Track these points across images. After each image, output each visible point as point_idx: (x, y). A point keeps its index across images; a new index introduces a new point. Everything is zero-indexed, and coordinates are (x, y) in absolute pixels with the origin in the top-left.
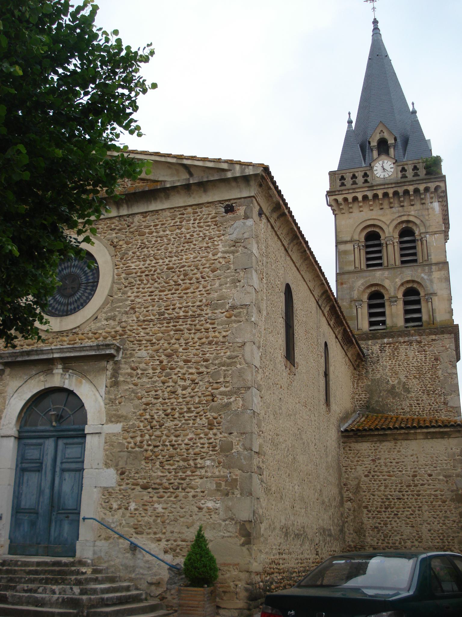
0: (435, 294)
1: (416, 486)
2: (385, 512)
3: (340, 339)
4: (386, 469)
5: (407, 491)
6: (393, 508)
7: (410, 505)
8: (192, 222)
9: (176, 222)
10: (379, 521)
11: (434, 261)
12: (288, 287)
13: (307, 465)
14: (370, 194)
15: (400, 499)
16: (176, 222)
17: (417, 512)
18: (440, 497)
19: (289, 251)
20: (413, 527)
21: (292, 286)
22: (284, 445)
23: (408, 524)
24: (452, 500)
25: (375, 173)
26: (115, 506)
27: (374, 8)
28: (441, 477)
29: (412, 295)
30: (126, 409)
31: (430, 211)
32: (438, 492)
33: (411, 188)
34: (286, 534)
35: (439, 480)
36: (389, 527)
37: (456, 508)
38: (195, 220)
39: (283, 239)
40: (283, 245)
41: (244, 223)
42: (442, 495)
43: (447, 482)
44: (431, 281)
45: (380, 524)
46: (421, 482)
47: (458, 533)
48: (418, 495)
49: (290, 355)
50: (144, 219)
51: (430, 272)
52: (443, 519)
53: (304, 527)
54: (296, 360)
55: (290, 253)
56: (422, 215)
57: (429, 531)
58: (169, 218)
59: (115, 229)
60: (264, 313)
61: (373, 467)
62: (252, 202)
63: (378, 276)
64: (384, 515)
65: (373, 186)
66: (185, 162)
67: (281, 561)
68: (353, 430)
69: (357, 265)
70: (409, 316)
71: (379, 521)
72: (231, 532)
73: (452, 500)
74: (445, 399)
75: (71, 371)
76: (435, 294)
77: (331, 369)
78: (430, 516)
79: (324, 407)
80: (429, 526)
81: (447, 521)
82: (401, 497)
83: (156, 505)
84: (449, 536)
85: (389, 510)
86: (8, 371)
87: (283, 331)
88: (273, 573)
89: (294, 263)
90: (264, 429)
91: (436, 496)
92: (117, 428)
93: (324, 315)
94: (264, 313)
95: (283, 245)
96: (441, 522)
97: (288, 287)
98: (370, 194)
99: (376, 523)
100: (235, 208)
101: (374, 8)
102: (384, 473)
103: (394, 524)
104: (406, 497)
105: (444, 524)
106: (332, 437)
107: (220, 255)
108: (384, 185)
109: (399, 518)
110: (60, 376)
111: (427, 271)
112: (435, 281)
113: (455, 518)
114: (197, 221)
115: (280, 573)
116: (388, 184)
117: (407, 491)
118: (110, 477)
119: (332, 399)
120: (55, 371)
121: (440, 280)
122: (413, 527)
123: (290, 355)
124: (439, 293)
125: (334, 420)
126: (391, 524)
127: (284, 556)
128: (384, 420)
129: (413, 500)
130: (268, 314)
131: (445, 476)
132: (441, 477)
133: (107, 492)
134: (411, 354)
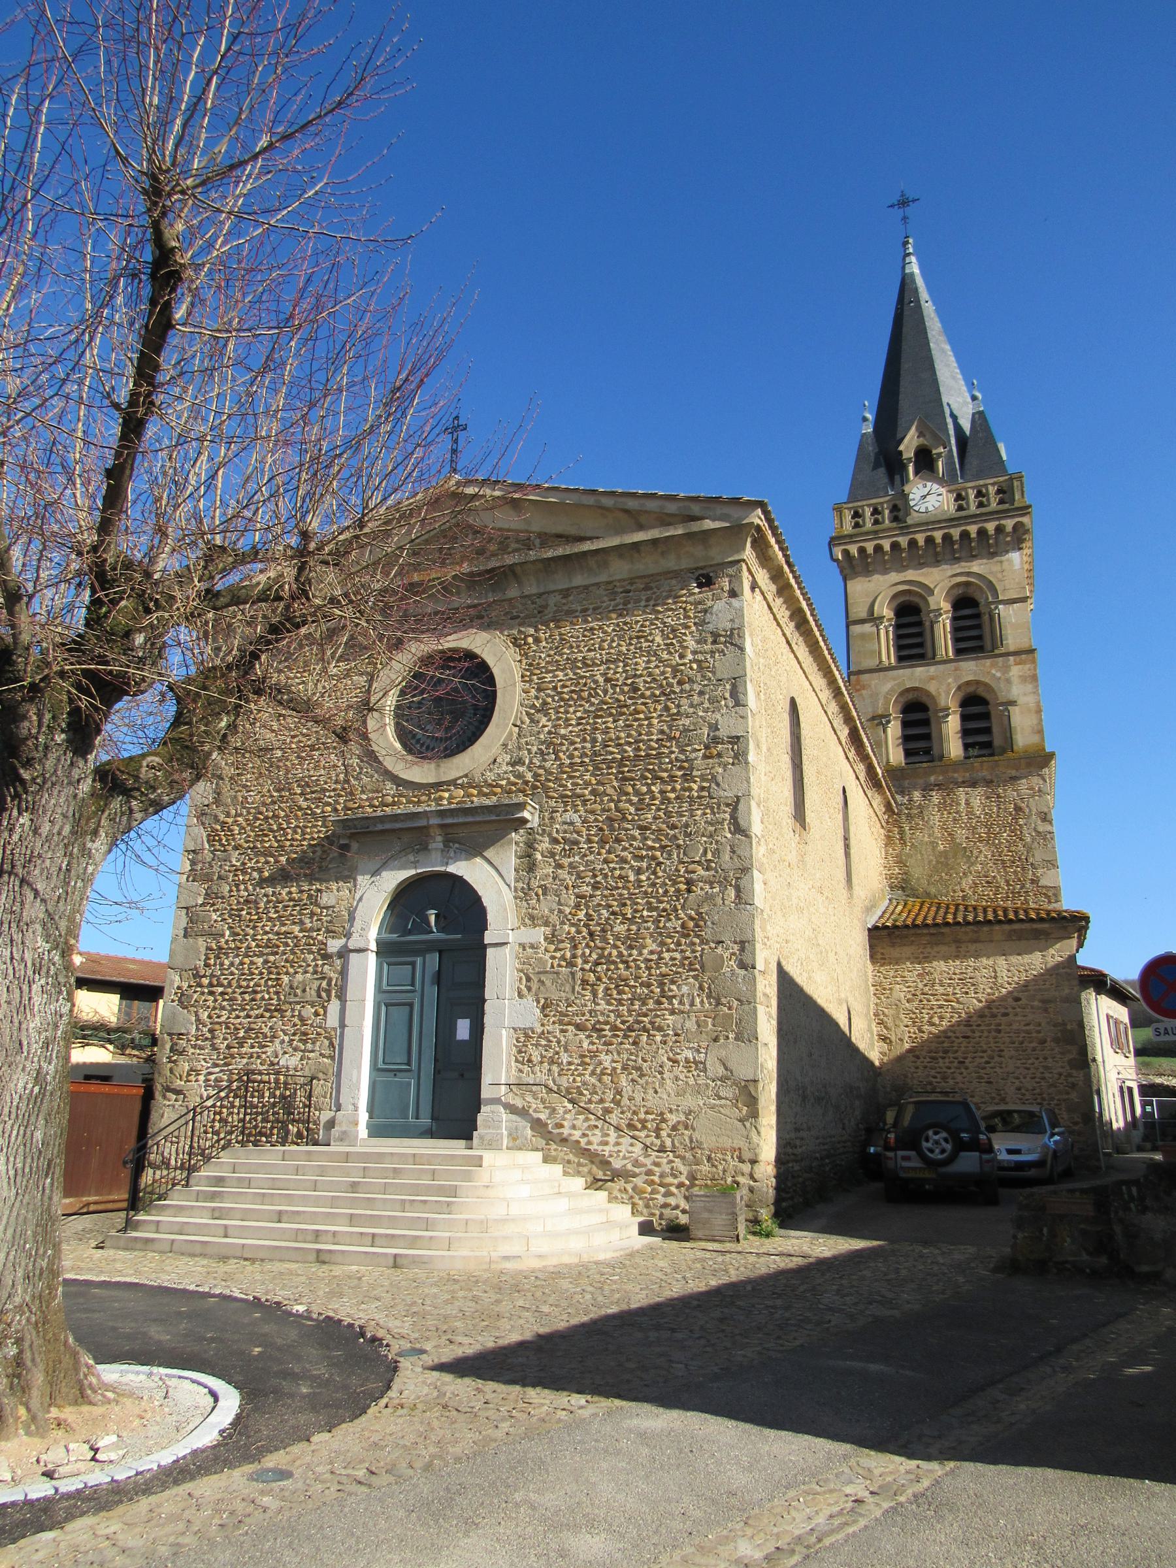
0: (1013, 703)
1: (994, 1016)
2: (943, 1058)
3: (862, 779)
4: (941, 990)
5: (979, 1025)
6: (956, 1051)
7: (985, 1047)
8: (643, 603)
9: (617, 605)
10: (933, 1072)
11: (1012, 649)
12: (793, 703)
13: (826, 987)
14: (903, 541)
15: (968, 1037)
16: (617, 605)
17: (997, 1059)
18: (1034, 1035)
19: (793, 645)
20: (990, 1083)
21: (798, 701)
22: (796, 957)
23: (980, 1077)
24: (1056, 1040)
25: (912, 503)
26: (536, 1058)
27: (905, 218)
28: (1036, 1003)
29: (979, 709)
30: (545, 907)
31: (1005, 565)
32: (1031, 1027)
33: (973, 529)
34: (804, 1098)
35: (1032, 1007)
36: (951, 1082)
37: (1062, 1053)
38: (648, 600)
39: (784, 626)
40: (784, 635)
41: (730, 604)
42: (1039, 1032)
43: (1046, 1010)
44: (1008, 681)
45: (935, 1077)
46: (1003, 1010)
47: (1068, 1093)
48: (999, 1031)
49: (799, 814)
50: (564, 601)
51: (1006, 669)
52: (1041, 1070)
53: (825, 1087)
54: (807, 820)
55: (795, 647)
56: (991, 573)
57: (1019, 1089)
58: (605, 598)
59: (518, 617)
60: (764, 749)
61: (920, 985)
62: (740, 571)
63: (916, 676)
64: (941, 1065)
65: (908, 527)
66: (632, 504)
67: (798, 1142)
68: (885, 927)
69: (884, 658)
70: (970, 740)
71: (933, 1072)
72: (726, 1099)
73: (1056, 1040)
74: (1034, 874)
75: (457, 845)
76: (1013, 703)
77: (852, 829)
78: (1018, 1064)
79: (845, 892)
80: (1017, 1082)
81: (1047, 1075)
82: (969, 1034)
83: (603, 1056)
84: (1052, 1099)
85: (950, 1055)
86: (355, 846)
87: (788, 774)
88: (788, 1162)
89: (799, 663)
90: (770, 935)
91: (1028, 1032)
92: (538, 934)
93: (841, 743)
94: (764, 749)
95: (784, 635)
96: (1038, 1075)
97: (793, 703)
98: (903, 541)
99: (928, 1076)
100: (714, 580)
101: (905, 218)
102: (939, 997)
103: (959, 1078)
104: (977, 1034)
105: (1044, 1078)
106: (858, 943)
107: (690, 657)
108: (927, 524)
109: (967, 1068)
110: (439, 854)
111: (1000, 664)
112: (1015, 680)
113: (1061, 1070)
114: (652, 603)
115: (796, 1161)
116: (933, 523)
117: (979, 1025)
118: (528, 1013)
119: (854, 880)
120: (432, 846)
121: (1024, 679)
122: (990, 1083)
123: (799, 814)
124: (1021, 700)
125: (858, 910)
126: (953, 1078)
127: (802, 1134)
128: (934, 909)
129: (991, 1040)
130: (769, 749)
131: (1043, 1001)
132: (1036, 1003)
133: (525, 1036)
134: (976, 802)
